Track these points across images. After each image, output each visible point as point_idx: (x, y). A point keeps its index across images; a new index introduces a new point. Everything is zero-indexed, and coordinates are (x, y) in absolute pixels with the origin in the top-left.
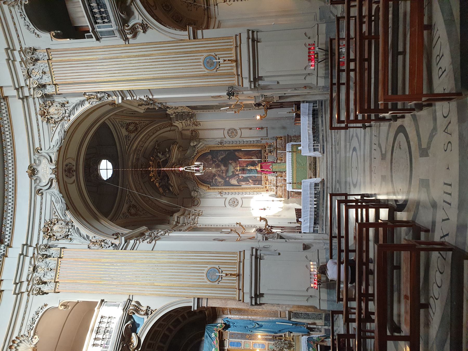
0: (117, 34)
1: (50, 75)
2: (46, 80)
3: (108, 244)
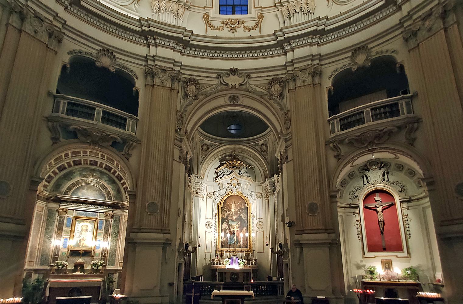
2: (299, 83)
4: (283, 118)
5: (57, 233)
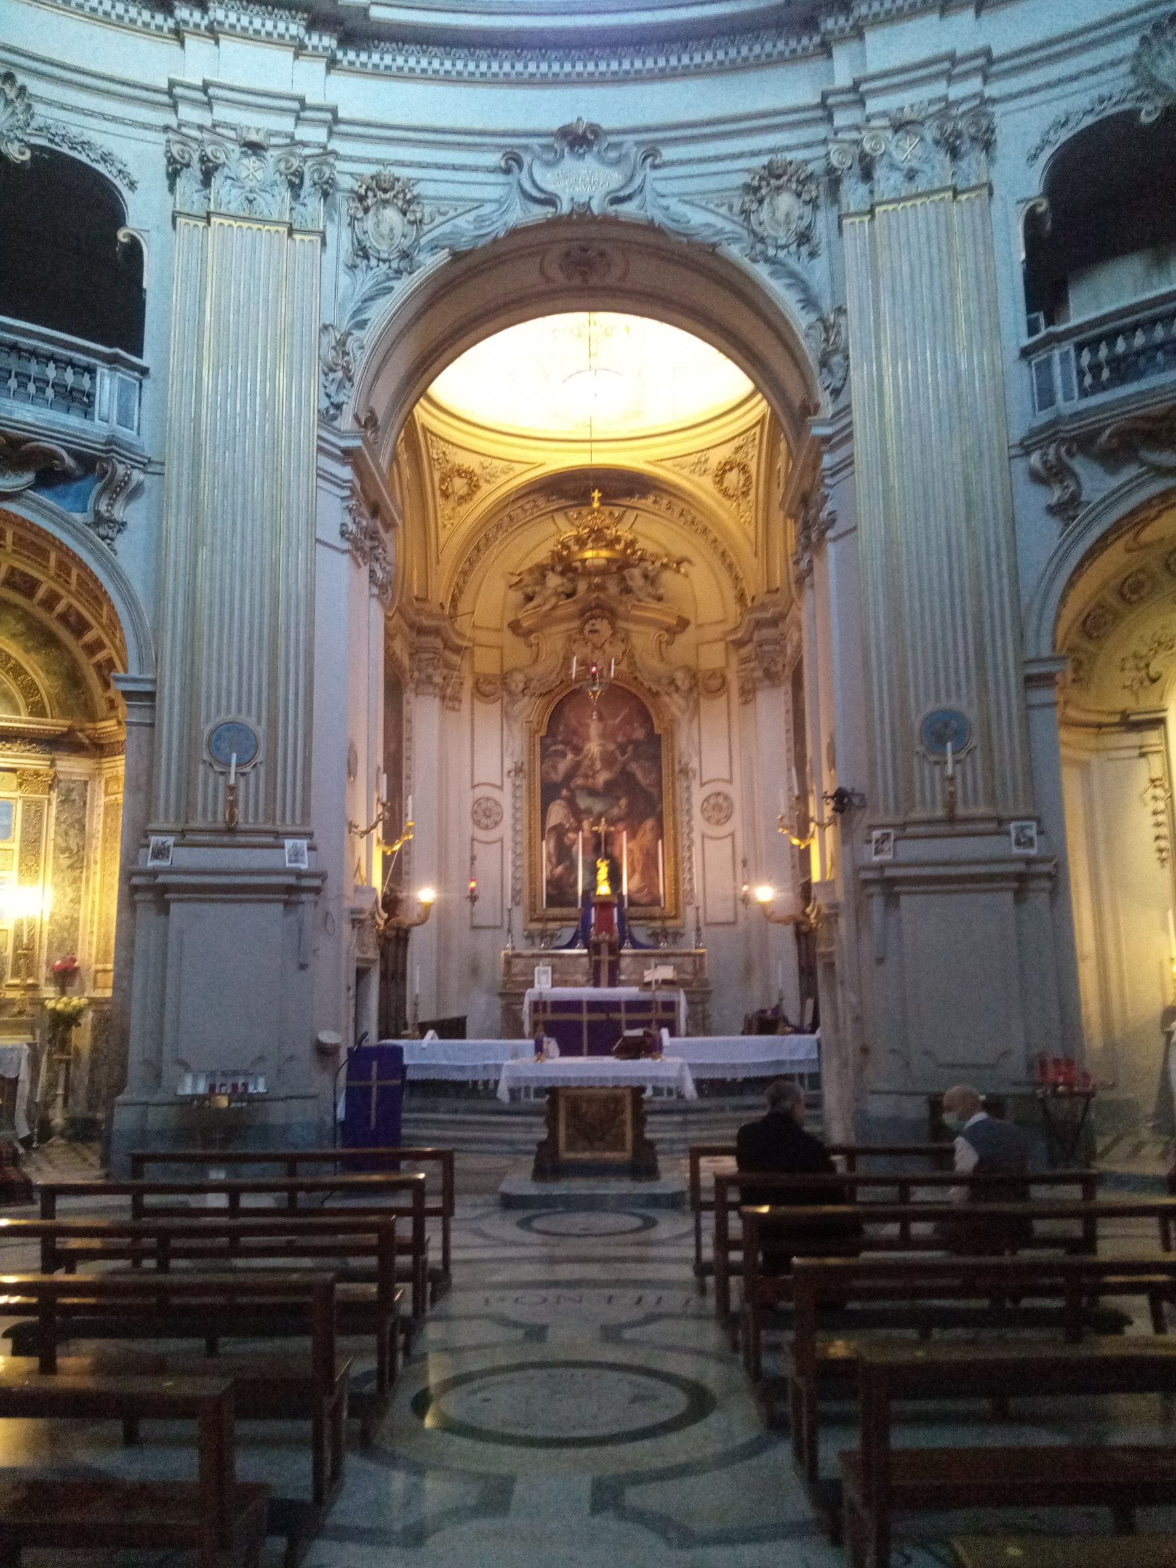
0: (1045, 417)
2: (887, 181)
3: (337, 392)
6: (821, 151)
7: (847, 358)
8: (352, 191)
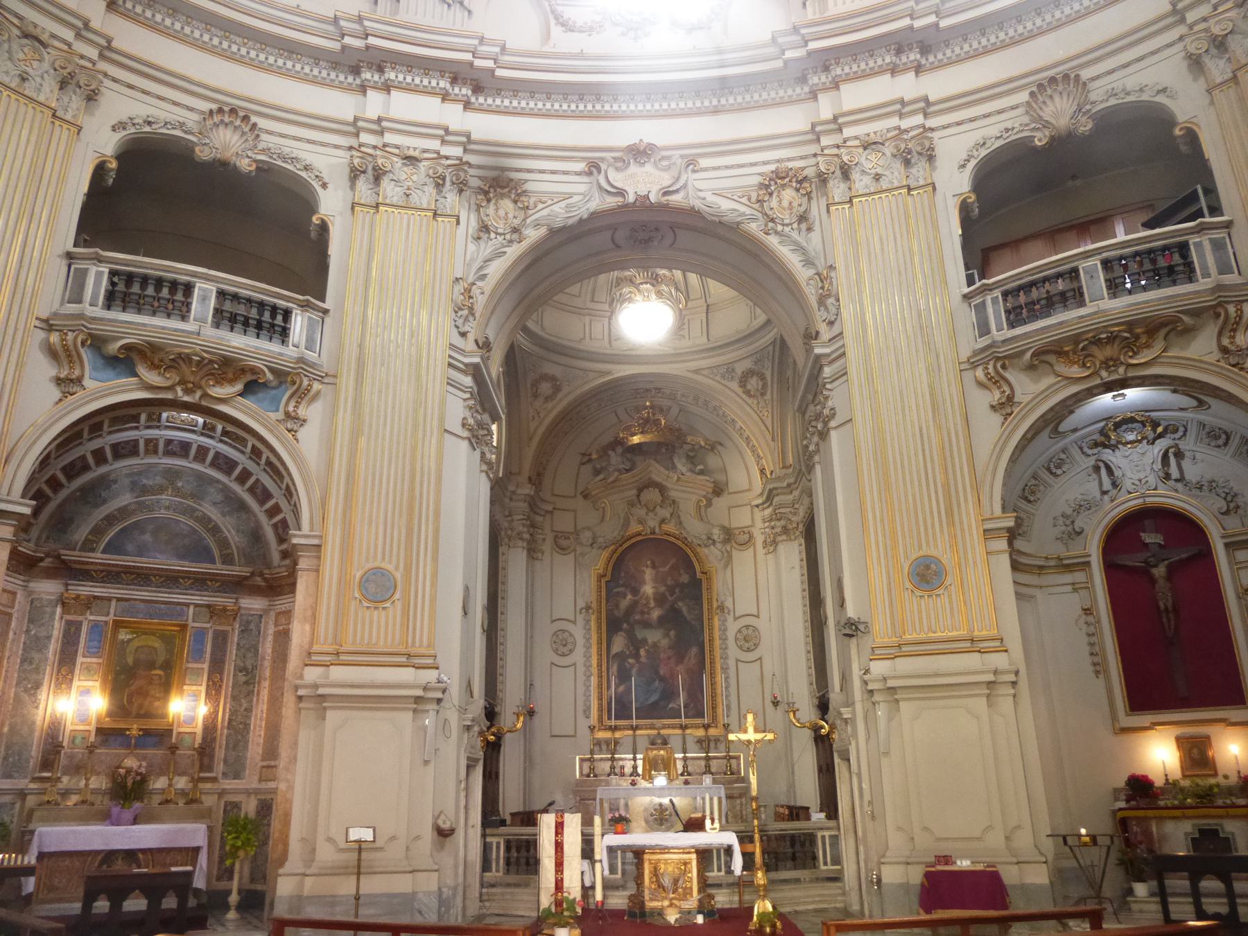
0: (983, 342)
1: (872, 190)
2: (861, 182)
3: (464, 324)
4: (813, 292)
5: (59, 671)
6: (812, 161)
7: (838, 300)
8: (480, 188)
